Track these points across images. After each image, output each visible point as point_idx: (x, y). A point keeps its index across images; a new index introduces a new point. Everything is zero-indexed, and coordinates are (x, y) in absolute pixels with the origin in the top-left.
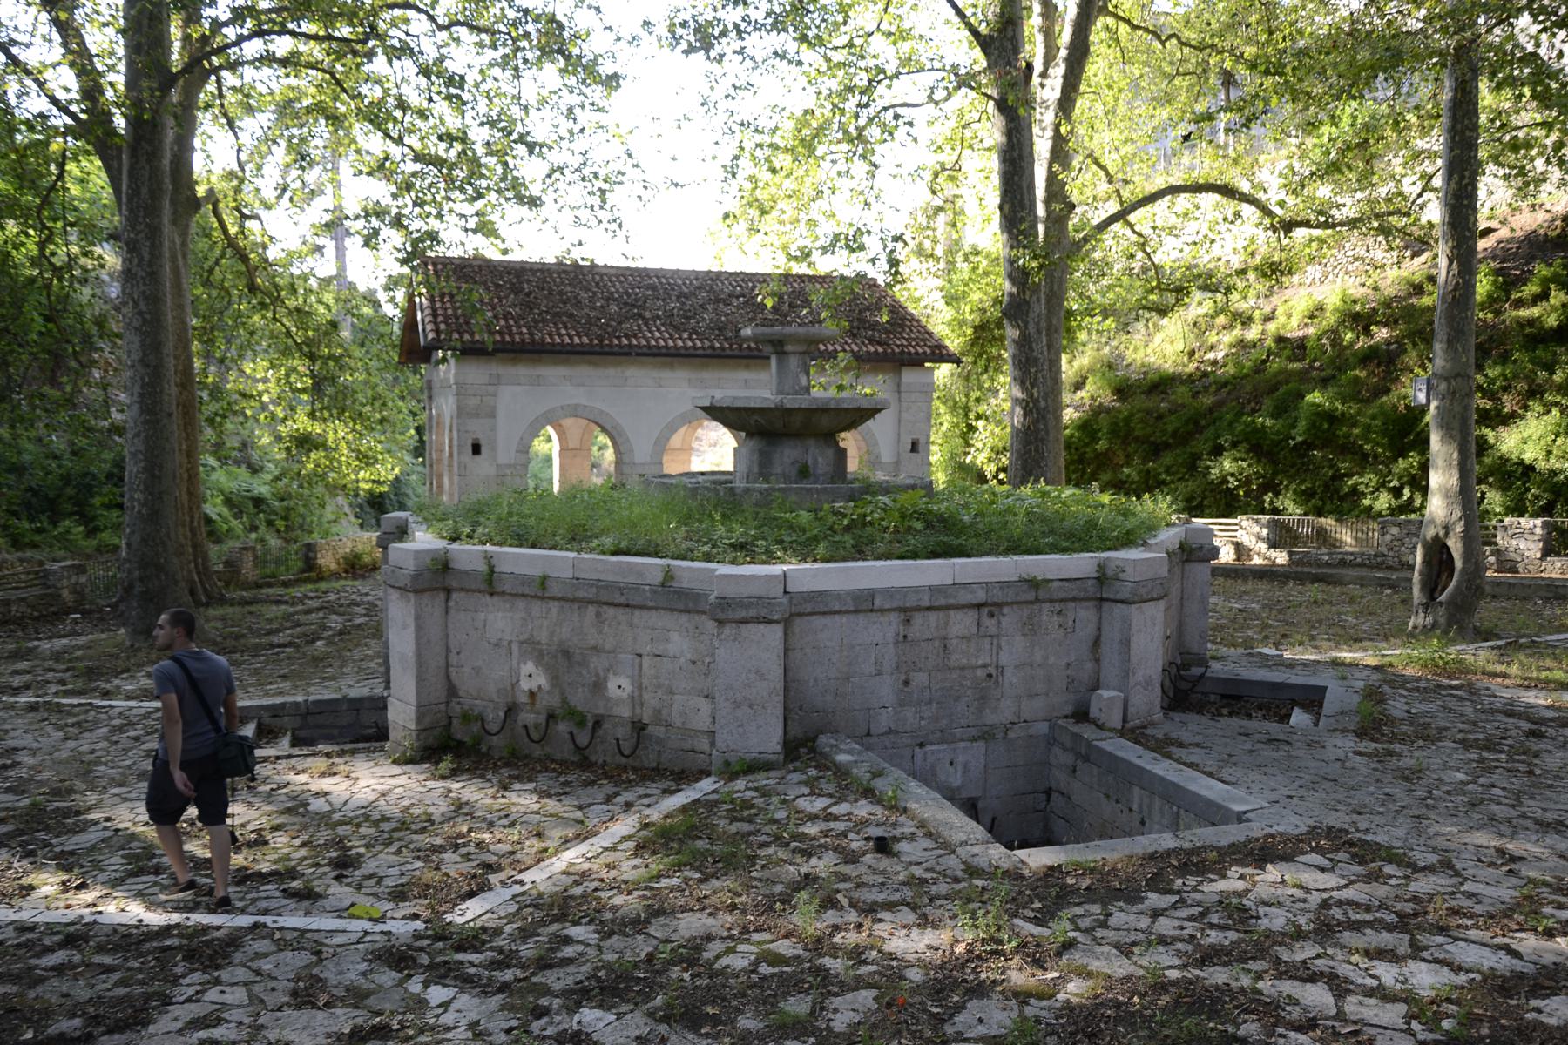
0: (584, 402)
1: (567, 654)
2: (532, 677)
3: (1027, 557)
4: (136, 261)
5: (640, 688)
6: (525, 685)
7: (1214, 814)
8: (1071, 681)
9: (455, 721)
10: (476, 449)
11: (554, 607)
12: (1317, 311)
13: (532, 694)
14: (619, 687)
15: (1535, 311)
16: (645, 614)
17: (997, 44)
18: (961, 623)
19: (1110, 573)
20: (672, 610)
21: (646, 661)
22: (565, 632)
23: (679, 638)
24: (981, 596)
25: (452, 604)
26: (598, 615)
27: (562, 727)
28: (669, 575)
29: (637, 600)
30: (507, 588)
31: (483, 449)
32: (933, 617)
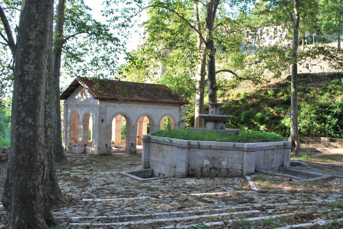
0: (123, 111)
1: (214, 158)
2: (207, 162)
3: (275, 142)
4: (56, 79)
5: (228, 163)
6: (205, 164)
7: (318, 176)
8: (281, 161)
9: (189, 171)
10: (102, 121)
11: (212, 150)
12: (239, 95)
13: (206, 165)
14: (224, 163)
15: (282, 98)
16: (230, 151)
17: (209, 44)
18: (270, 152)
19: (285, 144)
20: (235, 150)
21: (229, 159)
22: (214, 154)
23: (236, 155)
24: (272, 148)
25: (190, 150)
26: (221, 151)
27: (212, 170)
28: (234, 145)
29: (229, 149)
30: (203, 147)
31: (104, 121)
32: (267, 151)
